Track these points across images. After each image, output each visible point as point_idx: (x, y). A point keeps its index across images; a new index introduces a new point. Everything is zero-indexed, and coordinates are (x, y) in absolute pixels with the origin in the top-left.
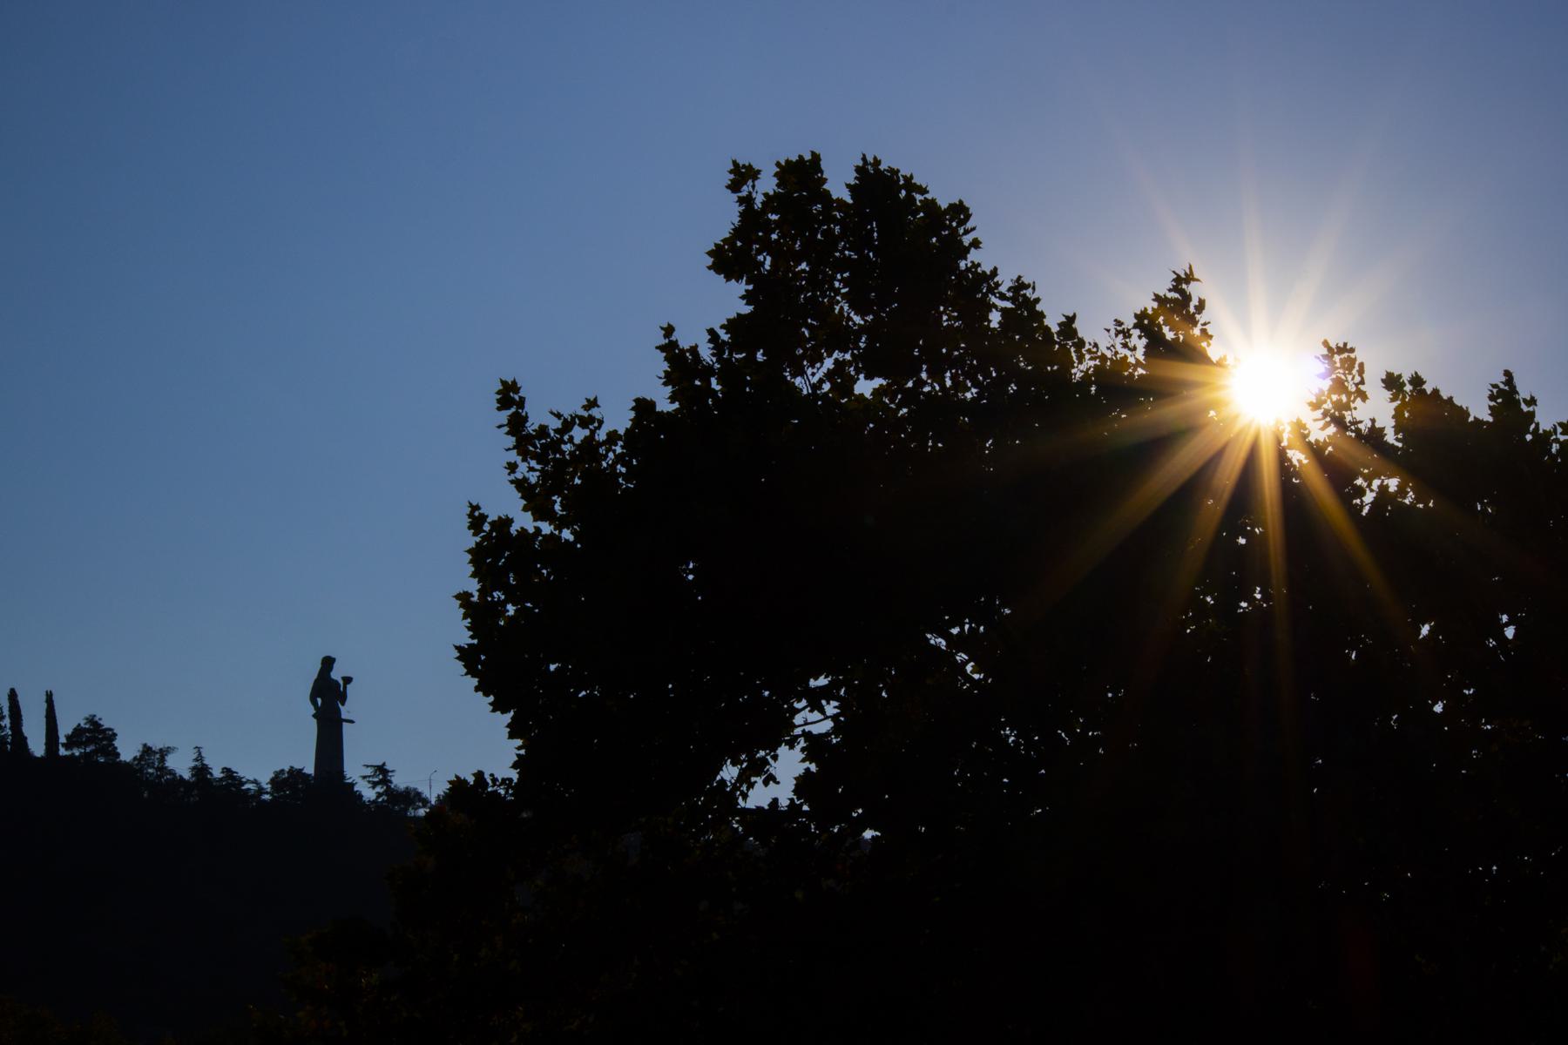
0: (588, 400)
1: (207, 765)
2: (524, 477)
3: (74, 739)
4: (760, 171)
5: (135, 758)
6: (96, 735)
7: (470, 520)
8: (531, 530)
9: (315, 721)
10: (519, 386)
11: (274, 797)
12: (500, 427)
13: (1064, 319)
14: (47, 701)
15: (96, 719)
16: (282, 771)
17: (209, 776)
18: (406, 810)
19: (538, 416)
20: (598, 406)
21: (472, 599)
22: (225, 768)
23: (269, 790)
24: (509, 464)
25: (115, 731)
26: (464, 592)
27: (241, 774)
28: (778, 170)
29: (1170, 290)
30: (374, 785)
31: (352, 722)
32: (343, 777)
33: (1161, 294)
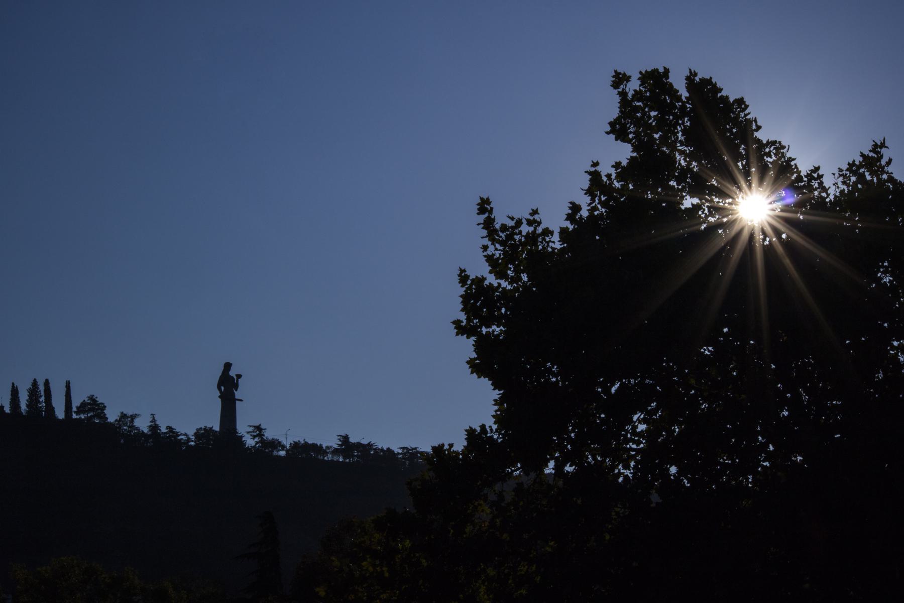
0: (533, 210)
1: (158, 425)
2: (493, 254)
3: (82, 409)
4: (631, 76)
5: (116, 420)
6: (94, 406)
7: (459, 278)
8: (496, 285)
9: (220, 400)
10: (490, 201)
11: (196, 443)
12: (478, 224)
13: (813, 168)
14: (66, 387)
15: (94, 397)
16: (201, 428)
17: (159, 431)
18: (272, 451)
19: (501, 219)
20: (538, 214)
21: (462, 324)
22: (168, 426)
23: (193, 439)
24: (483, 246)
25: (105, 405)
26: (458, 320)
27: (178, 430)
28: (641, 76)
29: (870, 151)
30: (254, 437)
31: (241, 400)
32: (237, 432)
33: (866, 154)
